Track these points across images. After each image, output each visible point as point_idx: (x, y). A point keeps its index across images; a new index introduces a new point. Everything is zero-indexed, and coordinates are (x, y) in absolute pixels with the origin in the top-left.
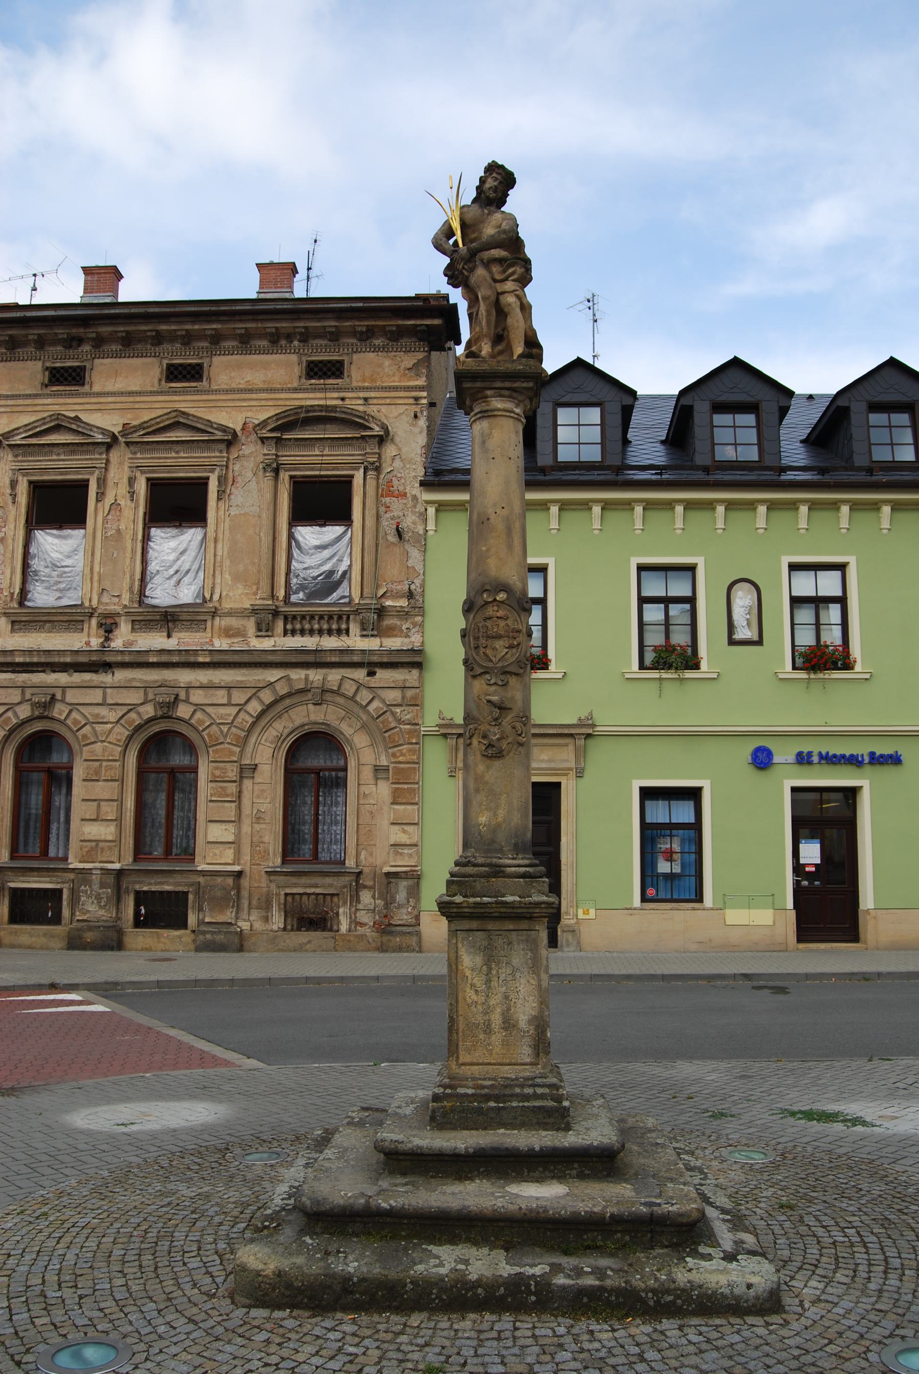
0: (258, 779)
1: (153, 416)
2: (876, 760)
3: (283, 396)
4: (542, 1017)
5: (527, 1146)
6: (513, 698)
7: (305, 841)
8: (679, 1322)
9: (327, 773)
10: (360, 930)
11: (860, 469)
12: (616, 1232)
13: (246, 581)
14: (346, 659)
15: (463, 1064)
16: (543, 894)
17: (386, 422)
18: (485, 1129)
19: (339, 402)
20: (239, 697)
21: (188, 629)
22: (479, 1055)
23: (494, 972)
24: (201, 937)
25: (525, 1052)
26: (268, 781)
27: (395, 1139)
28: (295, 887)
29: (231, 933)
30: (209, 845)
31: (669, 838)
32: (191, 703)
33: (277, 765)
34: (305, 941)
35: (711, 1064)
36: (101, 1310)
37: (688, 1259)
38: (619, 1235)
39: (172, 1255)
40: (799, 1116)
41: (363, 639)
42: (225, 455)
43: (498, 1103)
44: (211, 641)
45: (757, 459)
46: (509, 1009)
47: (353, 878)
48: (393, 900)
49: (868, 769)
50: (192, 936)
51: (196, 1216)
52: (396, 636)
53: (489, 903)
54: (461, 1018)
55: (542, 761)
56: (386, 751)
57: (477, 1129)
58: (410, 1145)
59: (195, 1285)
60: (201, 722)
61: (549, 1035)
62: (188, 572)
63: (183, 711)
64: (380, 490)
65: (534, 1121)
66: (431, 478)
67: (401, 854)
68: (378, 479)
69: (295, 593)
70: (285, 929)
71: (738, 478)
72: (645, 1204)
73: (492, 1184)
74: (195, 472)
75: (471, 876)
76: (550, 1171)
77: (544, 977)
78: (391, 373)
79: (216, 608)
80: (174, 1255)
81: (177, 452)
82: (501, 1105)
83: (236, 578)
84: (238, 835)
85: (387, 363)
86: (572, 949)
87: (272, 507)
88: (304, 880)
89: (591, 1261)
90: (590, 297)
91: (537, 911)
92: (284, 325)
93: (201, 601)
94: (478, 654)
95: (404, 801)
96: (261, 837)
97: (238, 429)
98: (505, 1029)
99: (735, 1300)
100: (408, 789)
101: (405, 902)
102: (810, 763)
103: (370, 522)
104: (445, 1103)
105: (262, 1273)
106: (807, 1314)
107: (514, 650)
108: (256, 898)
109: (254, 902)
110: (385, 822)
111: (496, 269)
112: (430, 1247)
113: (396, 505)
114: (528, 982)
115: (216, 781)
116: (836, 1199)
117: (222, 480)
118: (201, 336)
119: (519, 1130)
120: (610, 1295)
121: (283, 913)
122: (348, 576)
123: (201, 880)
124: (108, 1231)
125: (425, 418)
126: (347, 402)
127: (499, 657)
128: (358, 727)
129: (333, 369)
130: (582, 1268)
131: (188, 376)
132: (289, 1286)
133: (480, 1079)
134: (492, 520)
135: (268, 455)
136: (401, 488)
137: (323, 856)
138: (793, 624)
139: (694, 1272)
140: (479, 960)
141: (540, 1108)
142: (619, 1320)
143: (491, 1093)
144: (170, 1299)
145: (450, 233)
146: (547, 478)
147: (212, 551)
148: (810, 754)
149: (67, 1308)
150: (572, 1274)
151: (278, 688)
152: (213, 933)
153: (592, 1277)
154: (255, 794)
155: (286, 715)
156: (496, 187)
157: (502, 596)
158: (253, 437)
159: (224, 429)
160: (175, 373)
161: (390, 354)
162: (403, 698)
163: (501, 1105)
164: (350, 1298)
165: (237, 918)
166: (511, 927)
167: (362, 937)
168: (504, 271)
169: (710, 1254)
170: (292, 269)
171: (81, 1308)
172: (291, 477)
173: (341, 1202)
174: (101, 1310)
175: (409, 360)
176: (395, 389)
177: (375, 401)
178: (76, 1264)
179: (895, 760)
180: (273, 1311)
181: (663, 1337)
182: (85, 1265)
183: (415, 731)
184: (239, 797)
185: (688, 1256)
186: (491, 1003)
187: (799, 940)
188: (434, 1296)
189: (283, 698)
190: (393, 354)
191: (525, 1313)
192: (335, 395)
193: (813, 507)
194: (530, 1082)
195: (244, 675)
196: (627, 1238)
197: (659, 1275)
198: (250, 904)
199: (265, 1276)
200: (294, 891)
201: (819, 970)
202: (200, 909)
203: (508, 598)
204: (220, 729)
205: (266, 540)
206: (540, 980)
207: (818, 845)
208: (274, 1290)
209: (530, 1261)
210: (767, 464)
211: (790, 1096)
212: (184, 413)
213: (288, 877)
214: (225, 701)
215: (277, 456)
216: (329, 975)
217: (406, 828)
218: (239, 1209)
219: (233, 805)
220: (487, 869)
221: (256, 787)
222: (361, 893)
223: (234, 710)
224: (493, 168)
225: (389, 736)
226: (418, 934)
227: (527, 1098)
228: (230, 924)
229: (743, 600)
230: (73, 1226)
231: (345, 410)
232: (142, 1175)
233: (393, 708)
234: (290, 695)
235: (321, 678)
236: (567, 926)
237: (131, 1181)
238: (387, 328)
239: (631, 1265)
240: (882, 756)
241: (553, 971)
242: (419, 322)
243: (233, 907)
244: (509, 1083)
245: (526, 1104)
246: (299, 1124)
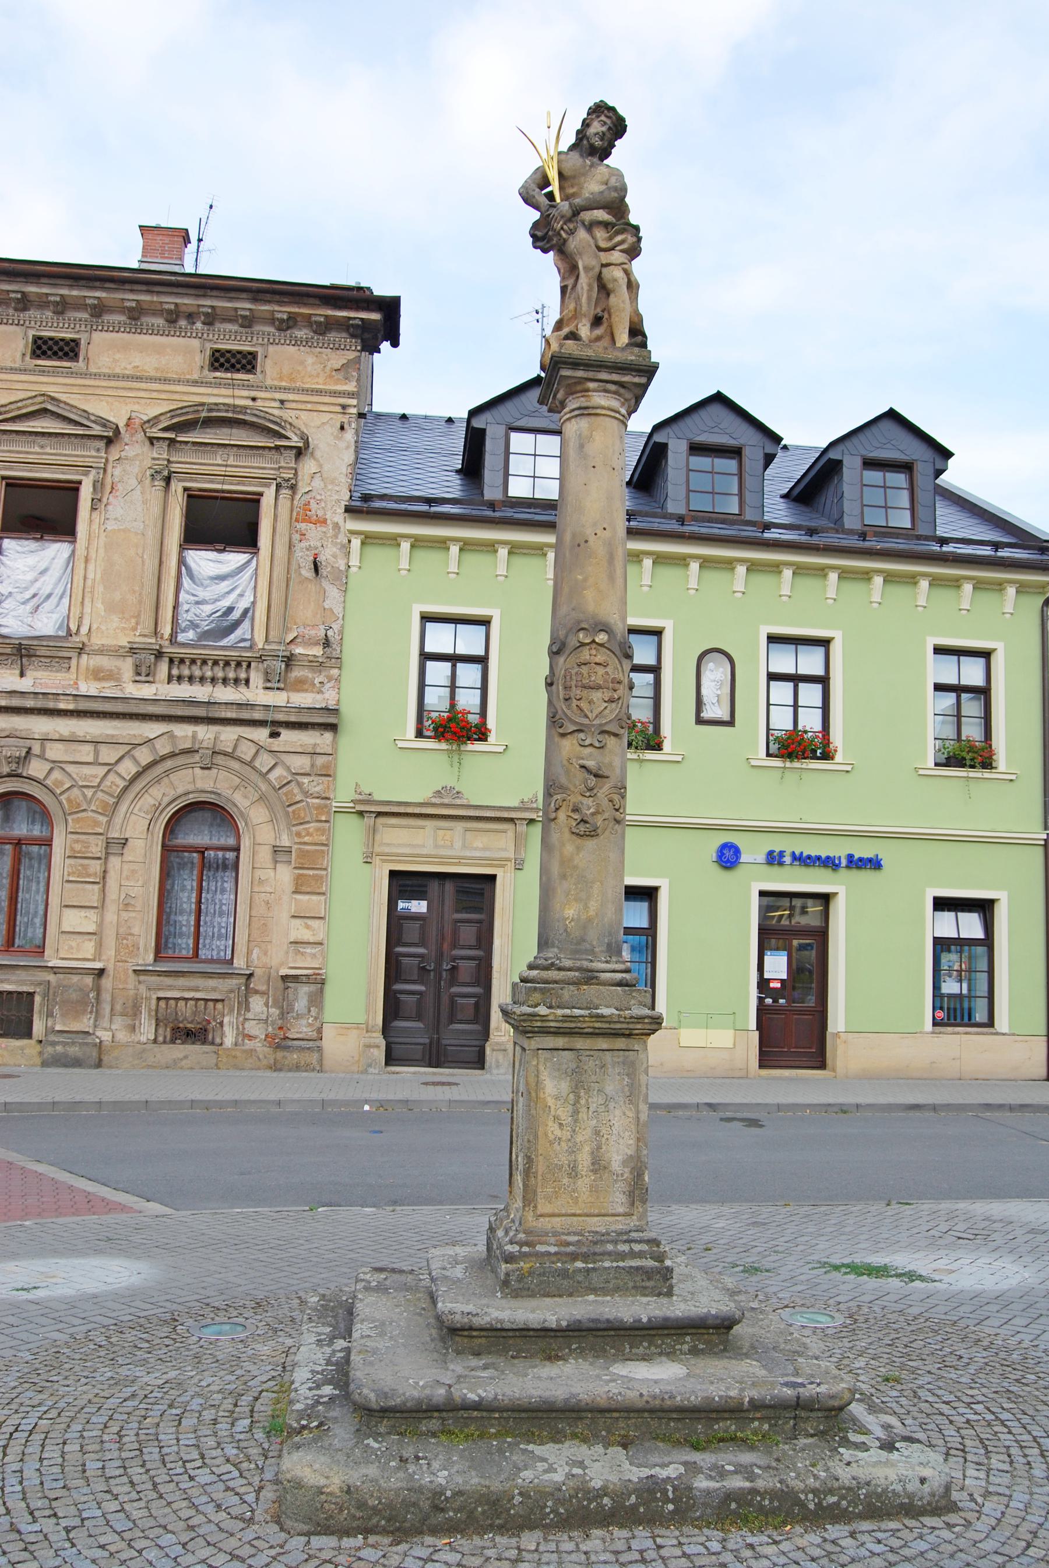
0: (129, 854)
1: (13, 399)
2: (855, 863)
3: (179, 388)
4: (639, 1157)
5: (632, 1316)
6: (610, 764)
8: (847, 1528)
10: (249, 1044)
11: (851, 532)
12: (754, 1419)
13: (123, 613)
14: (245, 715)
15: (541, 1216)
16: (645, 1006)
17: (305, 431)
18: (571, 1295)
19: (250, 403)
20: (109, 755)
21: (47, 667)
22: (562, 1204)
23: (583, 1102)
24: (50, 1049)
25: (618, 1201)
26: (141, 860)
27: (466, 1311)
28: (170, 990)
29: (87, 1044)
30: (64, 936)
32: (47, 760)
34: (181, 1056)
35: (712, 1210)
36: (102, 1547)
37: (841, 1450)
38: (756, 1423)
39: (169, 1466)
40: (843, 1270)
41: (267, 692)
42: (103, 455)
43: (587, 1263)
44: (76, 684)
45: (737, 512)
46: (599, 1147)
47: (243, 980)
48: (291, 1007)
49: (843, 873)
50: (38, 1048)
51: (178, 1411)
52: (306, 691)
53: (582, 1016)
54: (541, 1158)
55: (476, 849)
56: (289, 829)
58: (487, 1319)
59: (219, 1506)
60: (60, 783)
61: (646, 1179)
62: (49, 596)
63: (36, 768)
64: (295, 514)
65: (631, 1284)
66: (358, 504)
67: (302, 954)
68: (293, 500)
69: (183, 631)
70: (155, 1041)
71: (716, 531)
72: (786, 1384)
73: (591, 1364)
74: (63, 473)
75: (556, 982)
76: (657, 1347)
77: (643, 1108)
78: (314, 373)
79: (84, 644)
80: (172, 1465)
81: (42, 447)
82: (590, 1266)
83: (111, 608)
84: (101, 924)
85: (310, 360)
86: (502, 1071)
87: (160, 522)
88: (181, 981)
89: (730, 1457)
90: (539, 308)
92: (186, 301)
93: (64, 634)
94: (569, 707)
95: (309, 890)
96: (129, 927)
97: (121, 425)
98: (595, 1171)
99: (909, 1498)
100: (314, 876)
101: (305, 1011)
102: (781, 864)
103: (281, 551)
104: (522, 1264)
105: (325, 1490)
106: (985, 1510)
107: (614, 705)
108: (121, 1002)
109: (118, 1007)
110: (285, 916)
111: (600, 234)
112: (531, 1447)
113: (314, 533)
114: (624, 1114)
115: (76, 857)
116: (939, 1369)
117: (98, 486)
118: (80, 305)
119: (612, 1296)
120: (763, 1499)
121: (153, 1022)
122: (250, 614)
123: (52, 978)
124: (67, 1436)
125: (353, 431)
126: (259, 403)
127: (596, 712)
128: (255, 799)
129: (244, 361)
130: (723, 1466)
131: (60, 354)
132: (362, 1505)
133: (563, 1234)
134: (591, 543)
135: (158, 459)
136: (320, 513)
137: (203, 953)
138: (768, 705)
139: (854, 1465)
140: (565, 1086)
141: (637, 1268)
142: (776, 1528)
143: (579, 1251)
144: (191, 1528)
145: (545, 182)
146: (497, 514)
147: (82, 572)
148: (781, 854)
149: (55, 1546)
150: (713, 1474)
151: (158, 746)
152: (64, 1044)
153: (739, 1477)
154: (124, 875)
155: (166, 780)
156: (604, 134)
157: (602, 638)
158: (140, 436)
159: (104, 423)
160: (43, 348)
161: (313, 349)
162: (312, 766)
163: (590, 1266)
164: (440, 1517)
166: (605, 1046)
167: (252, 1051)
168: (610, 239)
169: (864, 1443)
170: (184, 236)
171: (73, 1545)
172: (185, 489)
173: (416, 1394)
174: (102, 1547)
175: (338, 359)
176: (319, 392)
177: (294, 405)
178: (42, 1483)
179: (875, 864)
180: (340, 1539)
181: (838, 1549)
182: (55, 1485)
183: (326, 806)
184: (104, 878)
185: (840, 1446)
186: (578, 1140)
187: (761, 1066)
188: (548, 1510)
189: (163, 758)
190: (318, 350)
191: (661, 1525)
192: (246, 393)
193: (798, 571)
194: (625, 1237)
195: (115, 728)
196: (766, 1426)
197: (816, 1472)
198: (112, 1010)
199: (330, 1494)
200: (169, 994)
201: (791, 1100)
202: (50, 1014)
203: (609, 640)
204: (84, 794)
205: (151, 564)
206: (638, 1112)
207: (785, 958)
208: (341, 1510)
209: (658, 1460)
210: (748, 517)
211: (821, 1247)
212: (53, 399)
213: (162, 978)
214: (90, 759)
215: (168, 461)
216: (219, 1098)
217: (310, 922)
218: (230, 1401)
219: (96, 887)
220: (577, 974)
221: (126, 867)
222: (251, 1000)
223: (101, 771)
224: (600, 109)
225: (294, 812)
226: (320, 1049)
227: (622, 1256)
228: (87, 1033)
229: (715, 675)
230: (16, 1430)
231: (257, 412)
232: (77, 1356)
233: (299, 778)
234: (173, 755)
235: (212, 736)
236: (497, 1043)
237: (67, 1366)
238: (314, 319)
239: (778, 1460)
240: (861, 859)
241: (653, 1098)
242: (352, 314)
243: (91, 1012)
244: (601, 1238)
245: (621, 1264)
246: (252, 1286)
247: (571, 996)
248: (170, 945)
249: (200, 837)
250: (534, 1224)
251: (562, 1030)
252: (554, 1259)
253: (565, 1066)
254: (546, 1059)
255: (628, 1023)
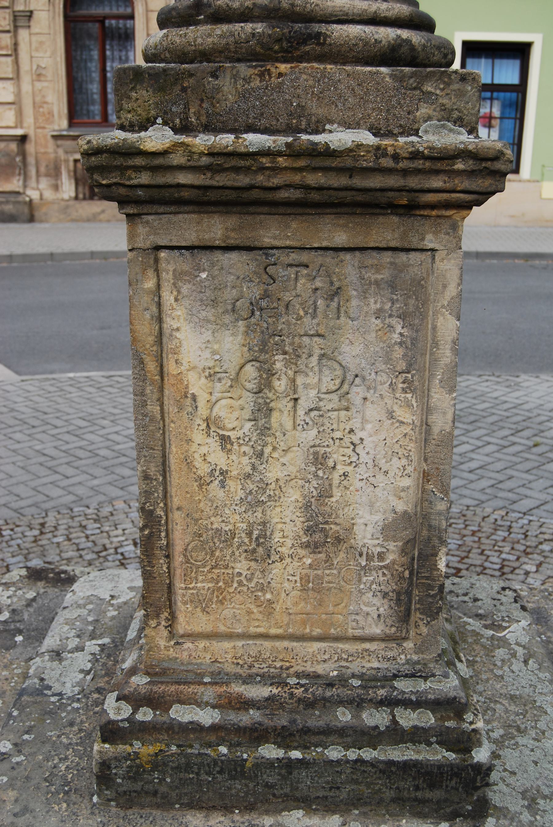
0: (35, 28)
4: (426, 517)
7: (93, 103)
9: (113, 22)
26: (46, 31)
31: (489, 102)
33: (54, 12)
43: (288, 748)
54: (177, 516)
57: (227, 809)
65: (389, 794)
70: (76, 198)
82: (296, 754)
84: (18, 94)
91: (437, 183)
96: (44, 97)
104: (137, 745)
109: (43, 169)
114: (391, 415)
121: (73, 181)
154: (34, 45)
163: (296, 754)
165: (25, 186)
194: (382, 692)
220: (259, 27)
221: (34, 38)
228: (18, 193)
245: (368, 754)
247: (244, 96)
248: (85, 112)
249: (101, 8)
250: (172, 653)
251: (212, 196)
252: (213, 738)
253: (230, 294)
254: (178, 276)
255: (405, 173)
